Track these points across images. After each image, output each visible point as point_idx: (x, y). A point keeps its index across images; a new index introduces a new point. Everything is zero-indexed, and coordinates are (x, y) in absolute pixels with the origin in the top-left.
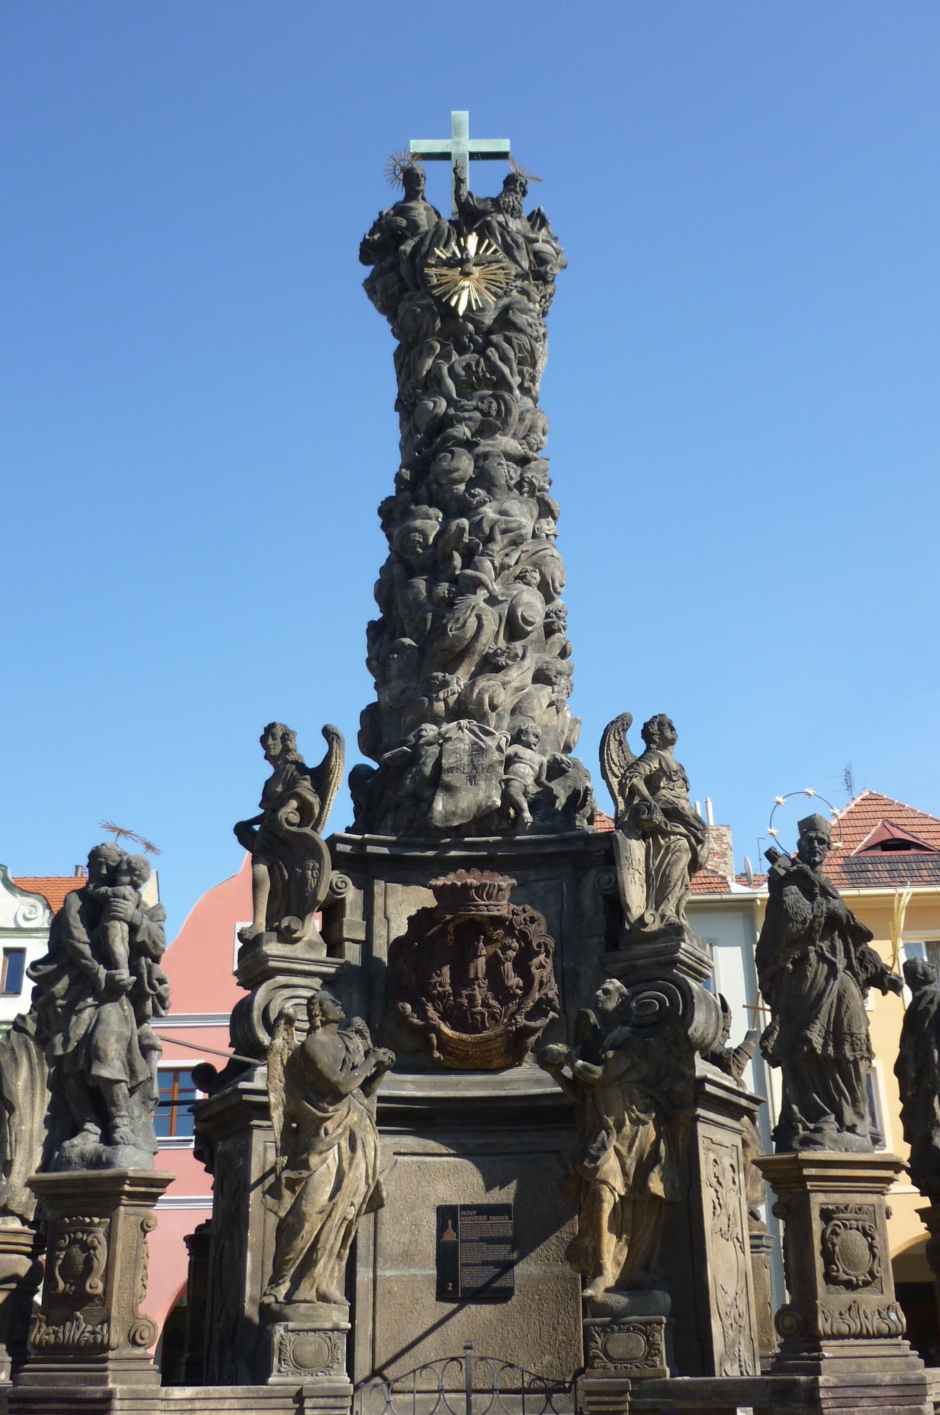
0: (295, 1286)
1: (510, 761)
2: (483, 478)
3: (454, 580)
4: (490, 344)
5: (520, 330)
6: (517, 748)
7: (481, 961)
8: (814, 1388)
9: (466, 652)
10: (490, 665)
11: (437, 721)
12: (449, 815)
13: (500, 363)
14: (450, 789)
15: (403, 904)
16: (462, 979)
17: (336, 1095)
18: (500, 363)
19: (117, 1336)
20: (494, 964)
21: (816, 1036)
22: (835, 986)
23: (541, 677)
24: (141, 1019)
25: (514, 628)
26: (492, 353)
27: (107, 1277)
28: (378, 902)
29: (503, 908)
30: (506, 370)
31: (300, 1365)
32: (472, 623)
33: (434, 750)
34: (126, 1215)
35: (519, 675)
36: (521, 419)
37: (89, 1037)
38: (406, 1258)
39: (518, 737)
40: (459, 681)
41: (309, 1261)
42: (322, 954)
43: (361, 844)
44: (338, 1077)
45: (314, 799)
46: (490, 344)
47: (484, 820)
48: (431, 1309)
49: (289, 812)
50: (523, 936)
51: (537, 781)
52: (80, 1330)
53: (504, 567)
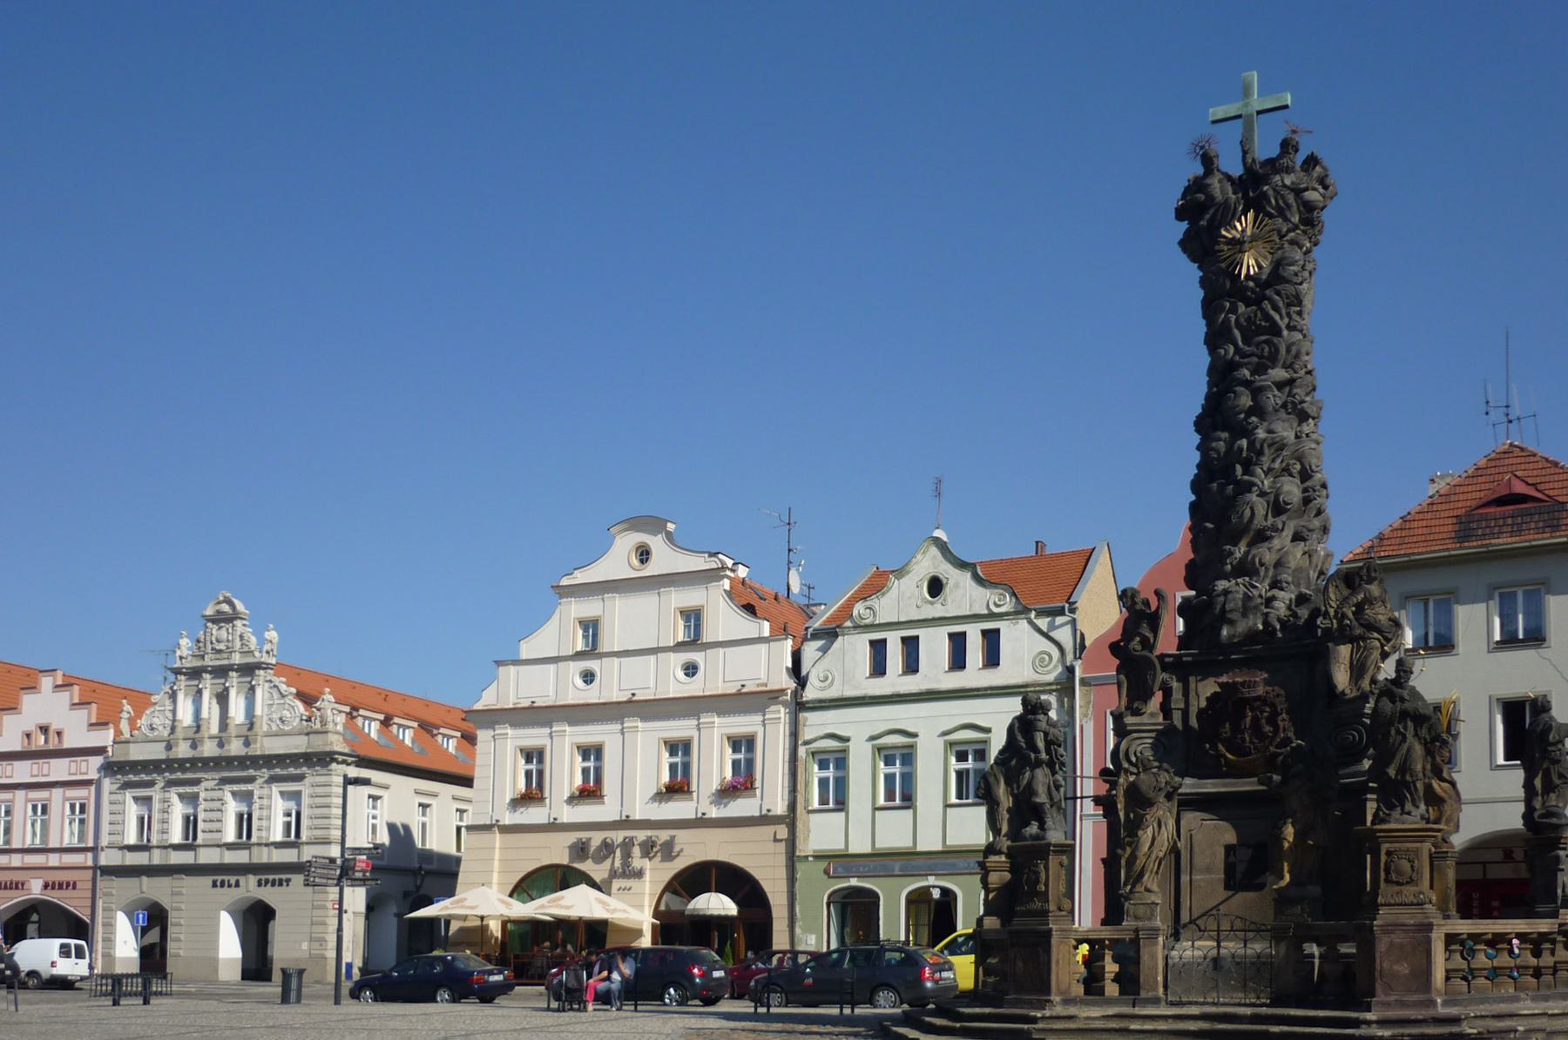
0: (1133, 886)
1: (1269, 601)
2: (1258, 410)
3: (1238, 483)
4: (1265, 298)
5: (1288, 282)
6: (1275, 592)
7: (1248, 720)
8: (1372, 926)
9: (1245, 529)
10: (1262, 537)
11: (1226, 577)
12: (1231, 637)
13: (1272, 313)
14: (1231, 623)
15: (1207, 688)
16: (1237, 729)
17: (1150, 803)
18: (1272, 313)
19: (1052, 907)
20: (1255, 720)
21: (1392, 772)
22: (1405, 747)
23: (1298, 537)
24: (1054, 773)
25: (1278, 508)
26: (1266, 305)
27: (1046, 885)
28: (1192, 686)
29: (1260, 690)
30: (1277, 317)
31: (1137, 918)
32: (1248, 512)
33: (1222, 599)
34: (1053, 861)
35: (1282, 541)
36: (1288, 351)
37: (1030, 783)
38: (1208, 870)
39: (1276, 584)
40: (1240, 551)
41: (1141, 874)
42: (1160, 719)
43: (1180, 656)
44: (1152, 795)
45: (1150, 636)
46: (1265, 298)
47: (1252, 636)
48: (1222, 894)
49: (1135, 644)
50: (1273, 706)
51: (1289, 608)
52: (1037, 905)
53: (1270, 470)
